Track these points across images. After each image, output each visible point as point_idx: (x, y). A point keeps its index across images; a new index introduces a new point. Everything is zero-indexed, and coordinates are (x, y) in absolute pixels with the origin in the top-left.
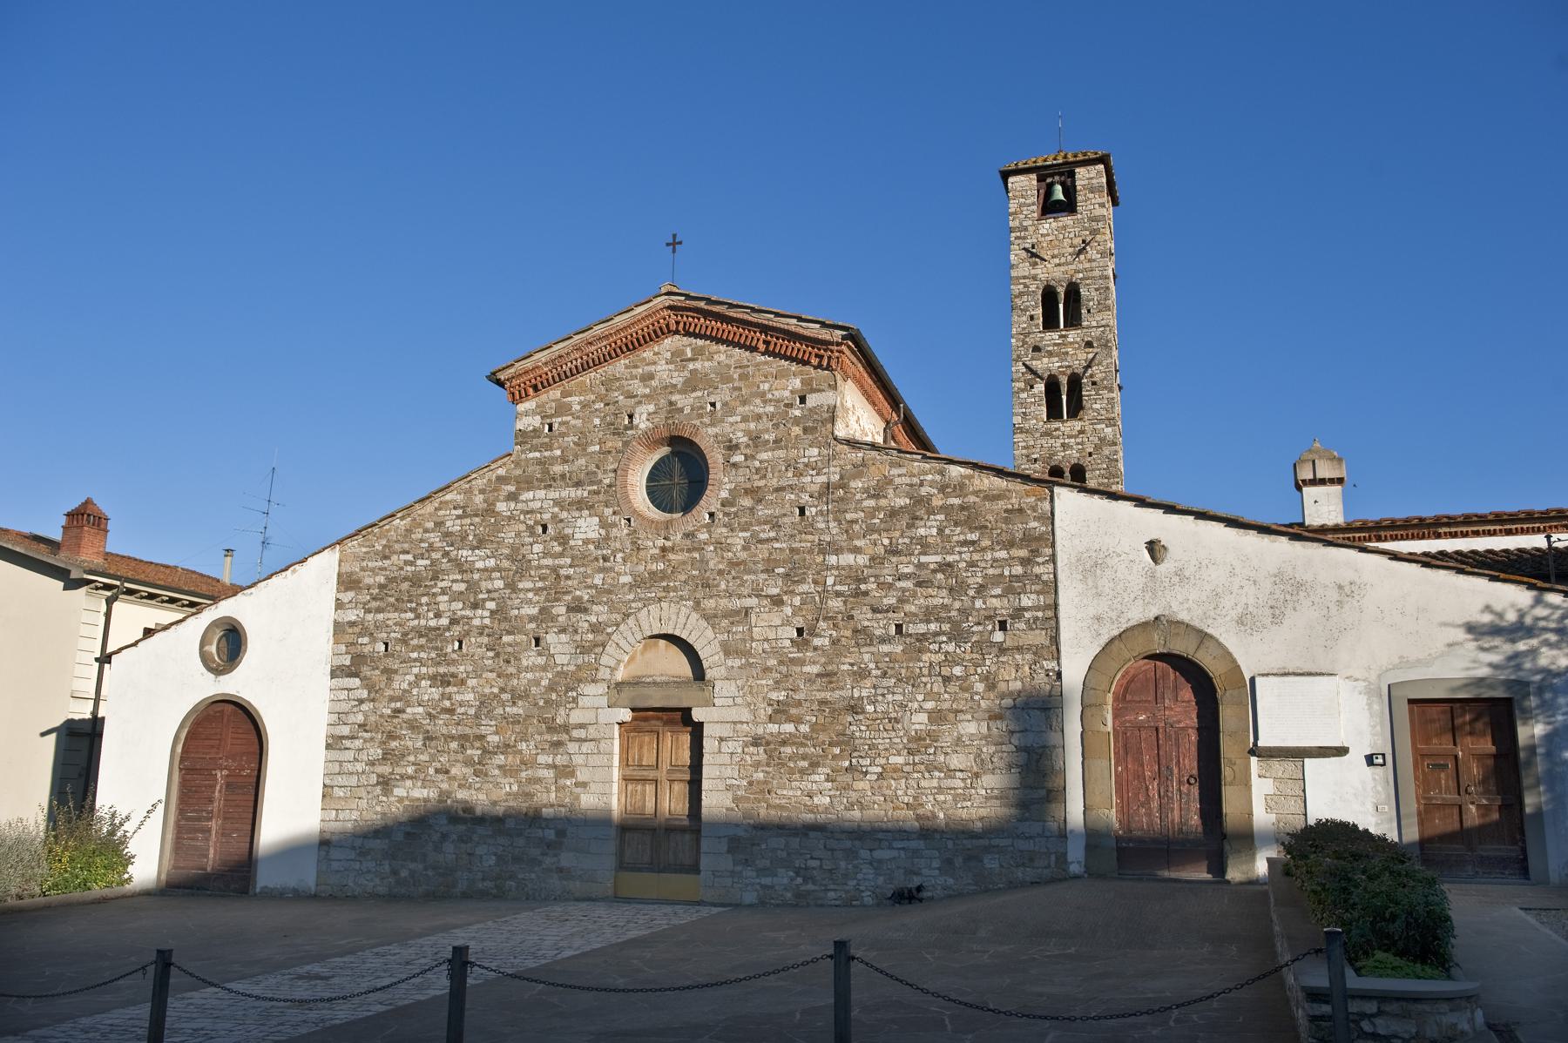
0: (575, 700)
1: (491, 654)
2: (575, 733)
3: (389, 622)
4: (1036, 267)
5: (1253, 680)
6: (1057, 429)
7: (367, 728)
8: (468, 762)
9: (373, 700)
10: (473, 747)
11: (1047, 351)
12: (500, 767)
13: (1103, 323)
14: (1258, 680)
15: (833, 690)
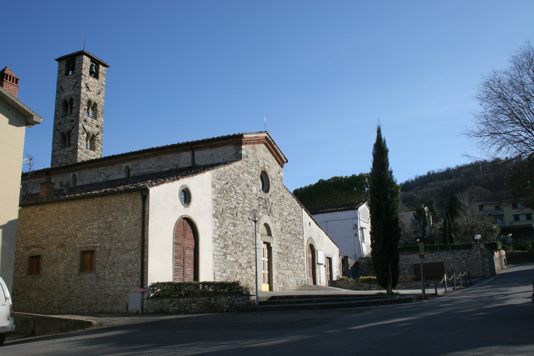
1: (242, 220)
3: (223, 203)
11: (88, 124)
12: (245, 254)
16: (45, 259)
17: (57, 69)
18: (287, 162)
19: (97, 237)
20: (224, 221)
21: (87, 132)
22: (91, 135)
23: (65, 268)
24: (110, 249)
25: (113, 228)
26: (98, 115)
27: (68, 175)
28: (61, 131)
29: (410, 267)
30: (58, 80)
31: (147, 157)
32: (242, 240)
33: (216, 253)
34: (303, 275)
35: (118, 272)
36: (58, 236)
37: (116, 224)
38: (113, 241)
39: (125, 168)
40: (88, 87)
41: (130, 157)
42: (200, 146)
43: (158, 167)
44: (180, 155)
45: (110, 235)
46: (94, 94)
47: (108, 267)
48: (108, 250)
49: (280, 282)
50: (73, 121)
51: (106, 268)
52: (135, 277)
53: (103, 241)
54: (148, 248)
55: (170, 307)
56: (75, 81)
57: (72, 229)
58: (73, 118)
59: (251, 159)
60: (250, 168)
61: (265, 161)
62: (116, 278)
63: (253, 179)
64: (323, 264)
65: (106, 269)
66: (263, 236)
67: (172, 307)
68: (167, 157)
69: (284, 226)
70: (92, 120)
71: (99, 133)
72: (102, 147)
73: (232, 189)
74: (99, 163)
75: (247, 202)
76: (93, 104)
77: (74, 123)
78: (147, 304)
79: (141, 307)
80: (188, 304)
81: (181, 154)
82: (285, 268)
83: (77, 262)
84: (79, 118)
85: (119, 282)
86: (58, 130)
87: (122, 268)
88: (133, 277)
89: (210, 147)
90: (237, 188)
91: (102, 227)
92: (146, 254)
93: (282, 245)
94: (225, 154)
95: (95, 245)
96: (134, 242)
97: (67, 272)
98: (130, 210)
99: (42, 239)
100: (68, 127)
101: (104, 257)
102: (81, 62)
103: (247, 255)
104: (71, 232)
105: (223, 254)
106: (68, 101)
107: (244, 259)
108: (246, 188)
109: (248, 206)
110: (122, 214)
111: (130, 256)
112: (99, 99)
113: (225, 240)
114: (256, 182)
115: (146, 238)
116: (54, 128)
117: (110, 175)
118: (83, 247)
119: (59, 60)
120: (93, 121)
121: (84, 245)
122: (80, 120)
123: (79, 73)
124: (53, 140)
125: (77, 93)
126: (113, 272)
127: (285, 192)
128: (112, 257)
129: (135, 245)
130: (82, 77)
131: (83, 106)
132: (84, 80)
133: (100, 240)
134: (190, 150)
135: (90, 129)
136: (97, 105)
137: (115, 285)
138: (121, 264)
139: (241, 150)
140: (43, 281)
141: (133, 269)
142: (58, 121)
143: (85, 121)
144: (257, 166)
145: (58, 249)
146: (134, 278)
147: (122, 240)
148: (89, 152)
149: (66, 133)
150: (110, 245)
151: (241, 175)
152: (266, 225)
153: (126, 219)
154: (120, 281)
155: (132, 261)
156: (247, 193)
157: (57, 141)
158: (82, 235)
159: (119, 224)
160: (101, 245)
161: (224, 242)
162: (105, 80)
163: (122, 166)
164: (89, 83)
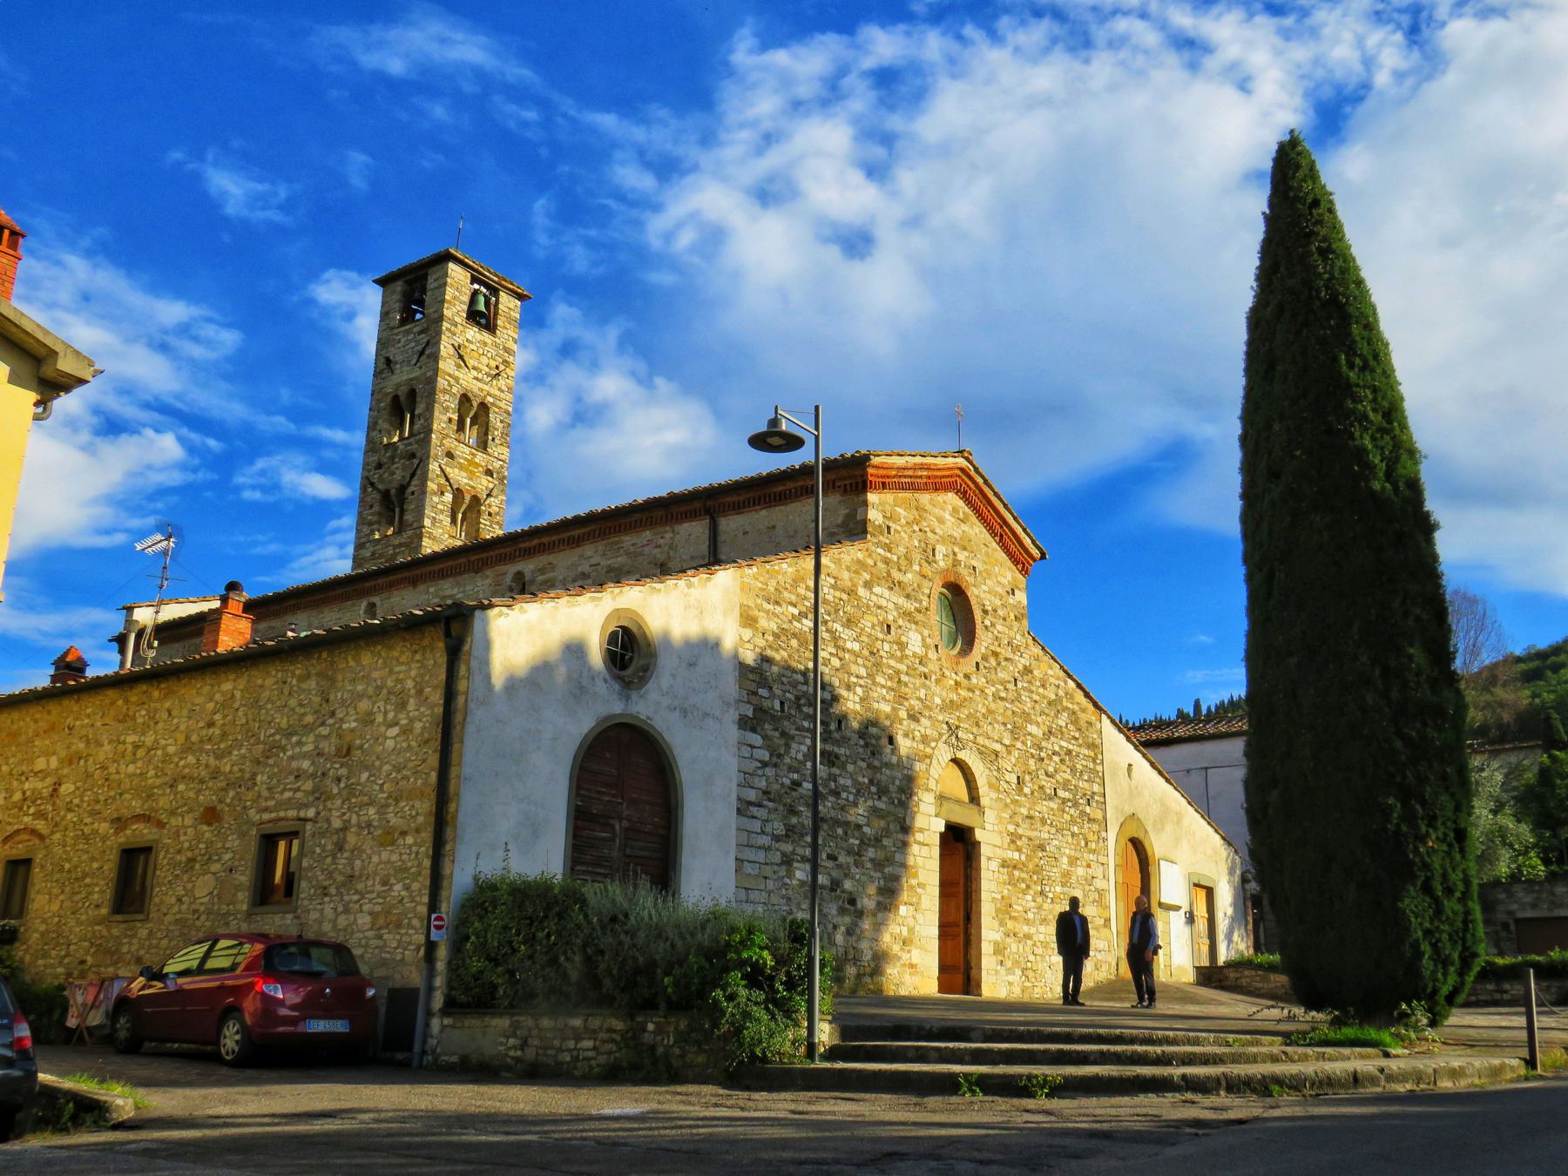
1: (862, 742)
3: (784, 679)
7: (772, 796)
8: (849, 852)
9: (775, 765)
10: (853, 837)
11: (460, 463)
12: (872, 860)
16: (162, 858)
18: (1043, 556)
19: (309, 786)
20: (788, 746)
21: (455, 487)
22: (467, 498)
23: (211, 893)
24: (345, 829)
26: (490, 438)
28: (380, 487)
29: (1499, 928)
31: (576, 542)
35: (361, 911)
36: (202, 781)
38: (354, 800)
39: (514, 580)
40: (461, 357)
41: (527, 544)
42: (735, 499)
43: (607, 572)
44: (673, 531)
45: (348, 778)
46: (480, 376)
47: (333, 891)
48: (338, 831)
49: (1009, 964)
50: (413, 456)
51: (326, 895)
52: (410, 931)
56: (424, 338)
57: (243, 757)
59: (906, 540)
60: (900, 570)
61: (956, 550)
62: (353, 932)
63: (910, 606)
64: (1181, 908)
65: (327, 899)
67: (514, 1047)
71: (494, 493)
74: (441, 566)
75: (883, 681)
76: (475, 404)
81: (677, 528)
82: (1031, 915)
83: (248, 872)
86: (372, 484)
88: (403, 931)
89: (765, 502)
90: (846, 634)
93: (1020, 837)
95: (302, 814)
98: (413, 692)
100: (398, 476)
101: (323, 855)
102: (441, 282)
104: (240, 770)
108: (881, 636)
109: (888, 697)
110: (389, 707)
111: (401, 854)
112: (497, 393)
113: (792, 811)
114: (919, 617)
118: (270, 821)
123: (436, 315)
127: (1037, 659)
128: (346, 855)
129: (418, 814)
131: (447, 409)
133: (317, 795)
134: (705, 515)
135: (466, 481)
140: (151, 933)
141: (405, 900)
142: (374, 458)
143: (450, 455)
144: (925, 564)
146: (406, 934)
147: (380, 796)
149: (393, 492)
150: (344, 814)
151: (862, 592)
153: (397, 724)
154: (363, 942)
155: (406, 870)
156: (882, 653)
160: (318, 813)
161: (785, 817)
162: (516, 336)
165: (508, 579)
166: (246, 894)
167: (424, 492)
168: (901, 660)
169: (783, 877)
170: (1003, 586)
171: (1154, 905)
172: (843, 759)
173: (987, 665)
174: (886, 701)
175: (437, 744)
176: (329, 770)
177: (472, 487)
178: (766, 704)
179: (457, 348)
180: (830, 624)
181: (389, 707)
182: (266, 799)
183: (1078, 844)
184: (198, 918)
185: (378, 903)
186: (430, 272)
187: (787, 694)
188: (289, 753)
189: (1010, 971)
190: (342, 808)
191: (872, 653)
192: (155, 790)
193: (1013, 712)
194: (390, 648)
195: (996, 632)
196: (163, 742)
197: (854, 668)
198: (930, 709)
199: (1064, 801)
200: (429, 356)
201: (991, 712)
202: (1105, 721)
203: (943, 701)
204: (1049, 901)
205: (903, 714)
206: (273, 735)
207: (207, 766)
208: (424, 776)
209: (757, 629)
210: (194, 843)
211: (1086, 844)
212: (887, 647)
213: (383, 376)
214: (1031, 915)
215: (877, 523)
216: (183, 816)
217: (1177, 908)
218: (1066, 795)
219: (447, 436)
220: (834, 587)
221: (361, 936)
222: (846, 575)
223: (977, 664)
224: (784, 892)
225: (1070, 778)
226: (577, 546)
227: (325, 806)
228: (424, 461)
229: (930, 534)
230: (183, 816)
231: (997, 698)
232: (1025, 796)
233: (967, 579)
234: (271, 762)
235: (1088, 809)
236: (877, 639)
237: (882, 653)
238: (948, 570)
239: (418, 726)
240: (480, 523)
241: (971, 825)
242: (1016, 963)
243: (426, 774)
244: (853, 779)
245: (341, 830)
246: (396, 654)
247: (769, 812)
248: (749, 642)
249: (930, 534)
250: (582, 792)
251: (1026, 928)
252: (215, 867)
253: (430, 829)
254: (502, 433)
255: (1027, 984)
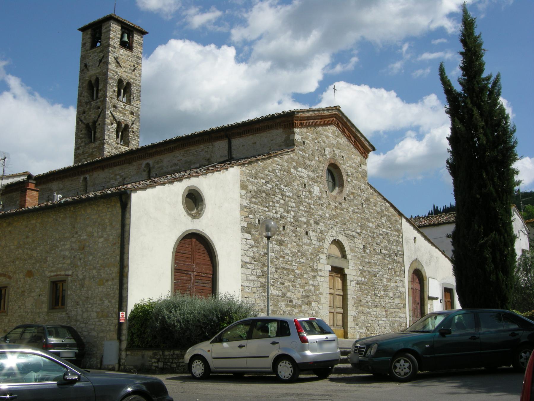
0: (319, 260)
1: (294, 235)
2: (320, 273)
3: (260, 210)
4: (118, 68)
5: (428, 278)
6: (120, 148)
7: (256, 259)
11: (119, 110)
12: (299, 284)
13: (138, 106)
14: (429, 279)
15: (371, 268)
17: (81, 41)
19: (68, 261)
21: (118, 120)
24: (84, 279)
25: (87, 248)
26: (132, 98)
27: (77, 178)
28: (85, 122)
30: (81, 57)
31: (171, 150)
32: (294, 264)
33: (246, 284)
34: (402, 315)
35: (93, 311)
36: (25, 260)
37: (91, 244)
38: (87, 267)
39: (145, 167)
40: (118, 63)
41: (151, 151)
43: (185, 163)
44: (213, 145)
45: (84, 259)
46: (127, 70)
47: (81, 303)
48: (81, 280)
49: (360, 325)
51: (78, 305)
53: (75, 268)
54: (127, 277)
55: (153, 363)
56: (101, 55)
58: (99, 104)
61: (335, 149)
62: (89, 319)
65: (78, 307)
66: (331, 258)
67: (155, 362)
68: (197, 150)
69: (369, 244)
70: (124, 105)
71: (135, 123)
72: (139, 140)
73: (277, 190)
75: (303, 208)
76: (125, 83)
77: (100, 110)
78: (126, 357)
79: (117, 362)
80: (176, 359)
81: (214, 144)
82: (370, 304)
83: (46, 296)
84: (106, 103)
85: (93, 324)
86: (81, 121)
87: (97, 305)
88: (109, 319)
89: (251, 132)
90: (286, 189)
91: (75, 247)
92: (125, 286)
93: (365, 271)
94: (272, 140)
95: (67, 273)
96: (112, 269)
97: (34, 310)
98: (108, 224)
99: (9, 264)
100: (93, 116)
102: (108, 29)
103: (302, 286)
104: (41, 256)
105: (259, 285)
106: (93, 82)
107: (296, 291)
108: (301, 189)
109: (305, 215)
110: (99, 230)
111: (107, 289)
112: (134, 77)
114: (319, 180)
115: (125, 263)
116: (77, 118)
117: (127, 177)
118: (54, 276)
119: (83, 29)
120: (125, 106)
121: (54, 272)
122: (107, 107)
123: (106, 44)
124: (77, 134)
125: (104, 71)
126: (87, 311)
128: (85, 289)
130: (109, 49)
131: (112, 86)
132: (112, 52)
135: (122, 118)
136: (131, 85)
137: (88, 329)
138: (96, 300)
139: (293, 135)
140: (9, 321)
141: (110, 307)
143: (115, 106)
144: (321, 157)
145: (26, 278)
146: (111, 320)
147: (97, 265)
148: (120, 148)
149: (91, 124)
150: (83, 273)
152: (337, 243)
153: (102, 237)
154: (94, 323)
156: (302, 196)
157: (81, 136)
158: (52, 258)
159: (95, 243)
160: (73, 273)
161: (261, 268)
163: (142, 164)
164: (120, 56)
165: (143, 166)
166: (46, 305)
167: (104, 124)
168: (310, 199)
169: (261, 293)
170: (356, 163)
171: (426, 297)
172: (286, 242)
173: (349, 198)
174: (304, 217)
175: (119, 245)
176: (76, 255)
177: (125, 120)
178: (252, 221)
179: (116, 59)
180: (279, 185)
181: (99, 230)
182: (52, 267)
183: (391, 273)
184: (28, 315)
185: (99, 308)
186: (103, 25)
187: (261, 216)
188: (60, 249)
189: (360, 328)
190: (82, 270)
191: (298, 196)
192: (7, 264)
193: (361, 218)
194: (99, 206)
195: (353, 184)
196: (9, 245)
197: (290, 203)
198: (324, 219)
199: (385, 255)
200: (104, 63)
201: (351, 218)
202: (404, 220)
203: (330, 215)
204: (378, 297)
205: (312, 222)
206: (53, 241)
207: (27, 254)
208: (114, 258)
209: (248, 190)
210: (24, 285)
211: (395, 273)
212: (304, 193)
213: (84, 72)
214: (370, 304)
215: (299, 141)
216: (19, 274)
217: (437, 299)
218: (386, 252)
219: (113, 98)
220: (280, 170)
221: (93, 320)
222: (285, 164)
223: (345, 198)
224: (262, 298)
225: (388, 245)
226: (172, 152)
227: (76, 270)
228: (104, 109)
229: (322, 144)
230: (19, 274)
231: (354, 212)
232: (367, 253)
233: (339, 162)
234: (53, 252)
235: (396, 258)
236: (300, 191)
237: (302, 196)
238: (331, 158)
239: (111, 237)
240: (129, 136)
241: (343, 267)
242: (364, 325)
243: (115, 257)
244: (290, 250)
245: (83, 279)
246: (101, 208)
247: (255, 266)
248: (244, 195)
249: (322, 144)
250: (178, 262)
251: (368, 310)
252: (33, 294)
253: (118, 278)
254: (137, 95)
255: (368, 333)
